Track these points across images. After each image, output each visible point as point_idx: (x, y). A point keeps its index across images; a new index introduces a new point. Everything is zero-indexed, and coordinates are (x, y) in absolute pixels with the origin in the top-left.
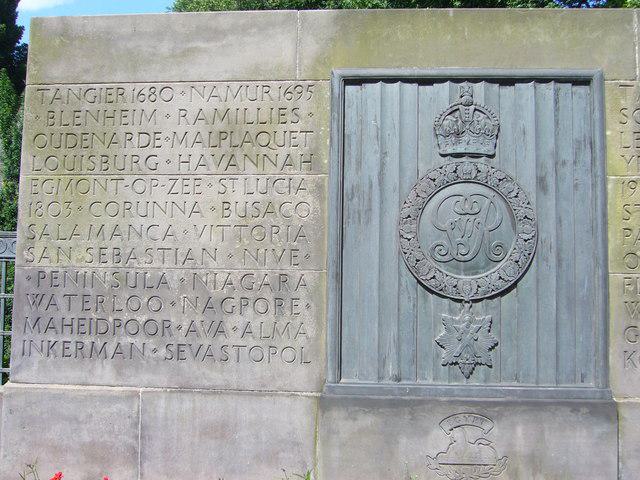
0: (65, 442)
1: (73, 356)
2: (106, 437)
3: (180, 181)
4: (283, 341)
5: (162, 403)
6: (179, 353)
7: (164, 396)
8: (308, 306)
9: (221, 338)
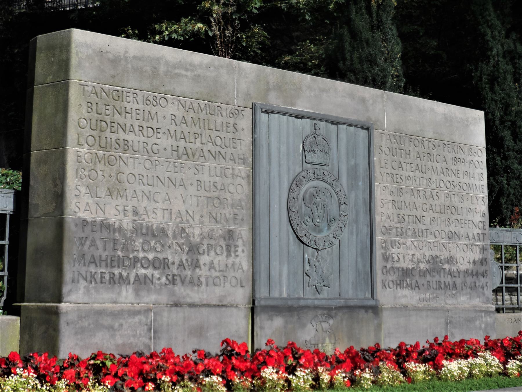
0: (105, 345)
1: (107, 283)
2: (132, 339)
3: (172, 163)
4: (231, 274)
5: (165, 314)
6: (173, 282)
7: (166, 309)
8: (243, 251)
9: (197, 270)
